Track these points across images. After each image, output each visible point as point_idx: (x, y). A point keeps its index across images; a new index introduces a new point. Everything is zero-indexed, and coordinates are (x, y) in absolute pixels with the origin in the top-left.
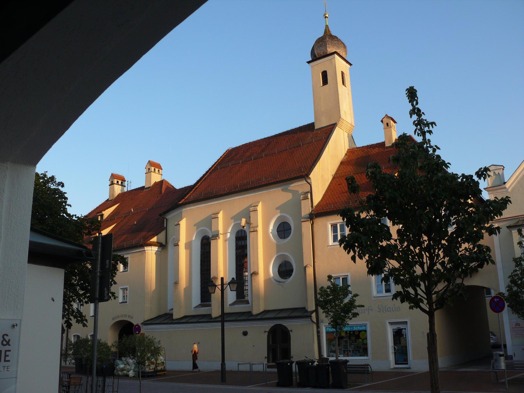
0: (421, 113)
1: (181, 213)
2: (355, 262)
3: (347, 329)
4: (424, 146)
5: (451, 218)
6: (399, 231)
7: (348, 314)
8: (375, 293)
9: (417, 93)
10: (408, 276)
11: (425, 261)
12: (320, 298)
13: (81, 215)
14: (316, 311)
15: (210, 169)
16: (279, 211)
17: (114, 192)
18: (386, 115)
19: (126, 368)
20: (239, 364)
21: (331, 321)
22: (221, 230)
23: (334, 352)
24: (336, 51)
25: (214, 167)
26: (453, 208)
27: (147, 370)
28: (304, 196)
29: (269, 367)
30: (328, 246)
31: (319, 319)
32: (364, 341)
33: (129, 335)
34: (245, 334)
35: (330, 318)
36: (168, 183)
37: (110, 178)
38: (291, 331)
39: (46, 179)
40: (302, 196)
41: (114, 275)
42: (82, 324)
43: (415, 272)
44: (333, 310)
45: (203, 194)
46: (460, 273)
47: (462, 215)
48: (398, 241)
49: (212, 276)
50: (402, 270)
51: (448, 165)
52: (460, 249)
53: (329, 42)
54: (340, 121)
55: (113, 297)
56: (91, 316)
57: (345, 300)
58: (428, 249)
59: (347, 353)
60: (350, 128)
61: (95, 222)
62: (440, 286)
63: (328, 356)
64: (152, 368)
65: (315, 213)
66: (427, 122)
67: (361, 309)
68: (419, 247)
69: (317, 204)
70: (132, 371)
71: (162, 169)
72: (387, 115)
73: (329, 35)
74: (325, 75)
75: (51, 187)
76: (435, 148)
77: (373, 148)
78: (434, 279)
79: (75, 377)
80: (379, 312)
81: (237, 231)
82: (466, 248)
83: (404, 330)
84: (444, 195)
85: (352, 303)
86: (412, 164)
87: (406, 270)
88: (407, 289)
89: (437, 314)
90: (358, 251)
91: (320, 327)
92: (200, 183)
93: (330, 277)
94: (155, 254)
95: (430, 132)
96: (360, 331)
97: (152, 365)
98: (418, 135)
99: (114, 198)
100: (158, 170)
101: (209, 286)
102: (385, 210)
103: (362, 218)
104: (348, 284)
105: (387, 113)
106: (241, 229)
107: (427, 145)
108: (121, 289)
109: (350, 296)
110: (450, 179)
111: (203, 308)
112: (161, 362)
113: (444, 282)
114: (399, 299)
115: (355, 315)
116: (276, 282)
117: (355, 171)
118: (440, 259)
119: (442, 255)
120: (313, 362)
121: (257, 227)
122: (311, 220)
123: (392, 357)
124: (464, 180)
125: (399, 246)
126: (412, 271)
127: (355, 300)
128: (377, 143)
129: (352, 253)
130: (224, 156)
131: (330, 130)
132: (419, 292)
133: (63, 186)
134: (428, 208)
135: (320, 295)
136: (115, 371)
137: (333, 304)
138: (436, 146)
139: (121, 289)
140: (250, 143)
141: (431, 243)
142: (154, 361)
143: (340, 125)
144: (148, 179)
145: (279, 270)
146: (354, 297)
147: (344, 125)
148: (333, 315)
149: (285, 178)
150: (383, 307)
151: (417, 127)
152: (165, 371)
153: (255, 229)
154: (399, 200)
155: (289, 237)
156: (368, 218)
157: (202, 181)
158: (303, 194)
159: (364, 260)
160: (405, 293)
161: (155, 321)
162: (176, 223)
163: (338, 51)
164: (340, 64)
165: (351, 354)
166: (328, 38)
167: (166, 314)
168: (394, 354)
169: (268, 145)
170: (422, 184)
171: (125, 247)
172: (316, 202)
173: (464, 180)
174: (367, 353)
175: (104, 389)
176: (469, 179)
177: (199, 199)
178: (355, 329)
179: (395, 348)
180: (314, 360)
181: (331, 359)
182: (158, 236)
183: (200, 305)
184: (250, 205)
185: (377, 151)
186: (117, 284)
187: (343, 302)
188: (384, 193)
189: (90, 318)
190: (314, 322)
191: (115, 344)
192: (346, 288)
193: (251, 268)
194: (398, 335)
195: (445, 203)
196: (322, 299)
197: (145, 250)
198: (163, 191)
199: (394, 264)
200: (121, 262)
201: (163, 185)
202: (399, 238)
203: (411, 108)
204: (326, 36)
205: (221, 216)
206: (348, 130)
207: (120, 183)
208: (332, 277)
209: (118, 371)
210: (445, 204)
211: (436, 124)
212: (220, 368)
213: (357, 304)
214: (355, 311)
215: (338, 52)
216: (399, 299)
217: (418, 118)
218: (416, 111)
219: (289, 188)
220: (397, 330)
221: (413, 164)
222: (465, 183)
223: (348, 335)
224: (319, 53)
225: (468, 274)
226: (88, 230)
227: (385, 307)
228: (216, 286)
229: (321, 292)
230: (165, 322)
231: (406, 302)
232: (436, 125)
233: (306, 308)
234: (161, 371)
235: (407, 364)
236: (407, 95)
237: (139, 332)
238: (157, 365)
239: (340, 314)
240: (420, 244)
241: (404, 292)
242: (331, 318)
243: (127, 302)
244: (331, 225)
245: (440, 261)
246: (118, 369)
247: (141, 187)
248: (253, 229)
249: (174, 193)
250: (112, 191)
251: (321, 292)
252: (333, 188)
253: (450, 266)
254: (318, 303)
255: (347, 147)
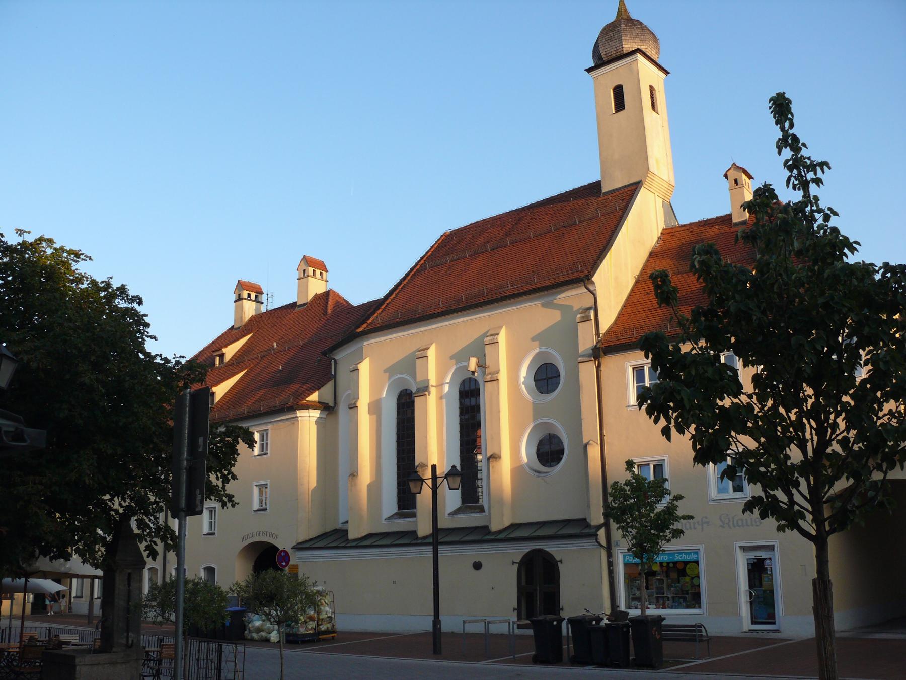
0: (800, 145)
1: (362, 348)
2: (669, 439)
3: (663, 558)
4: (806, 209)
5: (861, 351)
6: (756, 379)
7: (664, 532)
8: (713, 492)
9: (791, 106)
10: (775, 467)
11: (808, 436)
12: (611, 502)
13: (175, 355)
14: (606, 525)
15: (412, 269)
16: (537, 343)
17: (243, 313)
18: (734, 164)
19: (266, 627)
20: (464, 622)
21: (632, 544)
22: (433, 380)
23: (638, 599)
24: (639, 47)
25: (419, 266)
26: (866, 330)
27: (302, 630)
28: (582, 315)
29: (519, 627)
30: (627, 407)
31: (612, 541)
32: (694, 581)
33: (260, 571)
34: (477, 566)
35: (630, 538)
36: (338, 295)
37: (236, 289)
38: (561, 561)
39: (110, 290)
40: (579, 316)
41: (233, 462)
42: (175, 552)
43: (788, 457)
44: (637, 525)
45: (399, 314)
46: (880, 462)
47: (884, 345)
48: (754, 397)
49: (418, 461)
50: (762, 455)
51: (854, 245)
52: (881, 414)
53: (626, 32)
54: (648, 176)
55: (231, 503)
56: (204, 535)
57: (657, 505)
58: (814, 413)
59: (663, 601)
60: (666, 190)
61: (195, 367)
62: (842, 484)
63: (629, 607)
64: (310, 628)
65: (603, 346)
66: (812, 162)
67: (688, 522)
68: (796, 410)
69: (606, 330)
70: (275, 632)
71: (327, 271)
72: (735, 165)
73: (625, 19)
74: (619, 92)
75: (119, 306)
76: (829, 212)
77: (711, 225)
78: (827, 472)
79: (169, 645)
80: (721, 526)
81: (460, 380)
82: (891, 410)
83: (768, 561)
84: (847, 305)
85: (670, 511)
86: (781, 244)
87: (770, 455)
88: (772, 493)
89: (833, 542)
90: (674, 417)
91: (613, 553)
92: (394, 295)
93: (630, 465)
94: (316, 424)
95: (818, 182)
96: (686, 563)
97: (311, 622)
98: (794, 188)
99: (243, 324)
100: (321, 273)
101: (411, 480)
102: (729, 336)
103: (682, 352)
104: (664, 477)
105: (735, 162)
106: (469, 377)
107: (811, 208)
108: (256, 485)
109: (668, 498)
110: (859, 273)
111: (402, 520)
112: (326, 616)
113: (848, 479)
114: (756, 511)
115: (678, 533)
116: (532, 472)
117: (677, 268)
118: (838, 432)
119: (842, 425)
120: (599, 620)
121: (498, 372)
122: (595, 359)
123: (745, 610)
124: (889, 275)
125: (757, 407)
126: (782, 456)
127: (677, 506)
128: (717, 217)
129: (663, 422)
130: (437, 244)
131: (629, 193)
132: (797, 498)
133: (140, 303)
134: (814, 332)
135: (611, 497)
136: (246, 632)
137: (637, 513)
138: (830, 209)
139: (256, 485)
140: (484, 220)
141: (821, 401)
142: (314, 614)
143: (649, 185)
144: (303, 289)
145: (538, 450)
146: (675, 501)
147: (656, 185)
148: (637, 533)
149: (548, 283)
150: (729, 519)
151: (791, 172)
152: (334, 632)
153: (494, 377)
154: (755, 315)
155: (554, 390)
156: (694, 352)
157: (398, 290)
158: (580, 311)
159: (687, 435)
160: (769, 500)
161: (316, 543)
162: (352, 368)
163: (643, 48)
164: (647, 72)
165: (670, 604)
166: (624, 24)
167: (336, 531)
168: (749, 605)
169: (516, 224)
170: (802, 285)
171: (262, 412)
172: (605, 325)
173: (889, 275)
174: (700, 603)
175: (220, 666)
176: (898, 273)
177: (393, 323)
178: (678, 558)
179: (751, 594)
180: (601, 616)
181: (634, 613)
182: (320, 390)
183: (396, 514)
184: (485, 333)
185: (717, 231)
186: (237, 479)
187: (654, 510)
188: (726, 302)
189: (203, 537)
190: (602, 546)
191: (235, 588)
192: (659, 485)
193: (488, 447)
194: (758, 570)
195: (849, 321)
196: (615, 503)
197: (297, 417)
198: (329, 311)
199: (748, 442)
200: (245, 439)
201: (330, 300)
202: (757, 391)
203: (780, 135)
204: (619, 21)
205: (432, 353)
206: (663, 191)
207: (253, 297)
208: (635, 463)
209: (250, 632)
210: (848, 323)
211: (830, 166)
212: (430, 628)
213: (680, 512)
214: (676, 526)
215: (643, 50)
216: (756, 511)
217: (793, 155)
218: (790, 141)
219: (555, 301)
220: (755, 560)
221: (784, 244)
222: (890, 281)
223: (665, 569)
224: (608, 52)
225: (896, 462)
226: (183, 382)
227: (733, 518)
228: (423, 480)
229: (614, 492)
230: (334, 544)
231: (770, 517)
232: (830, 168)
233: (588, 520)
234: (327, 632)
235: (774, 623)
236: (772, 109)
237: (287, 563)
238: (320, 623)
239: (650, 531)
240: (799, 402)
241: (767, 497)
242: (632, 540)
243: (266, 509)
244: (633, 368)
245: (839, 438)
246: (251, 629)
247: (290, 304)
248: (490, 376)
249: (349, 313)
250: (239, 311)
251: (613, 491)
252: (637, 301)
253: (859, 447)
254: (609, 513)
255: (662, 225)
